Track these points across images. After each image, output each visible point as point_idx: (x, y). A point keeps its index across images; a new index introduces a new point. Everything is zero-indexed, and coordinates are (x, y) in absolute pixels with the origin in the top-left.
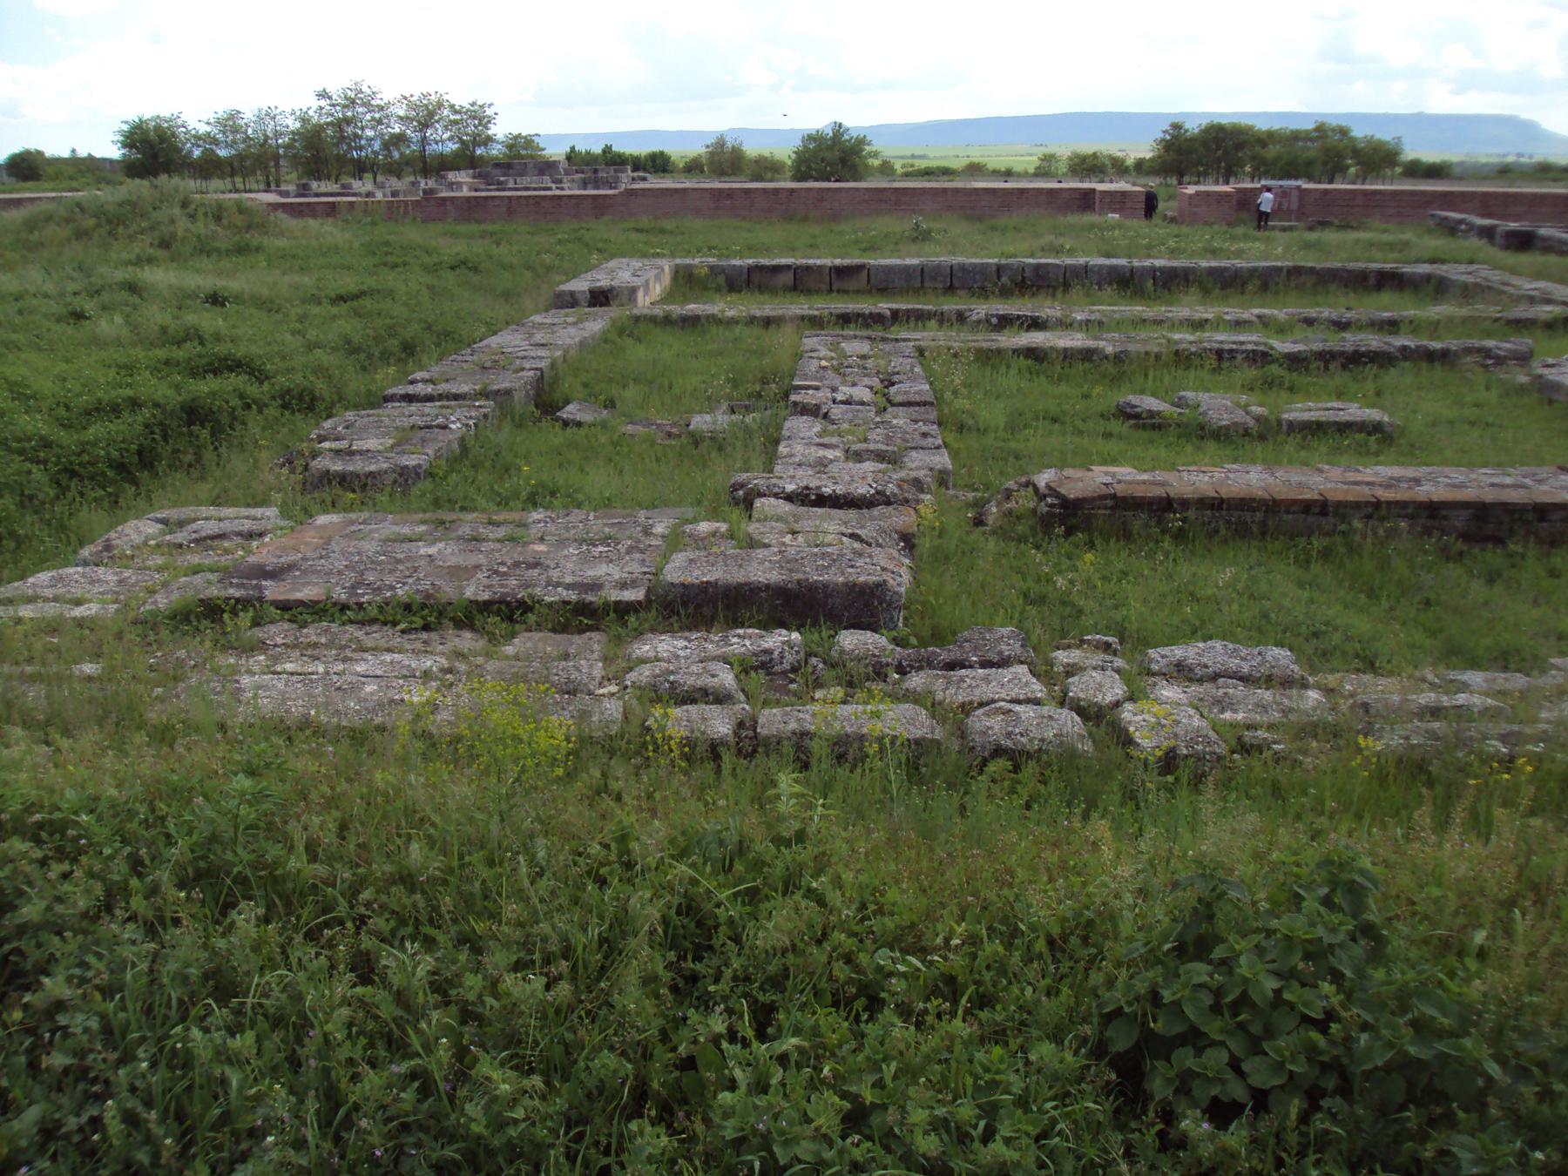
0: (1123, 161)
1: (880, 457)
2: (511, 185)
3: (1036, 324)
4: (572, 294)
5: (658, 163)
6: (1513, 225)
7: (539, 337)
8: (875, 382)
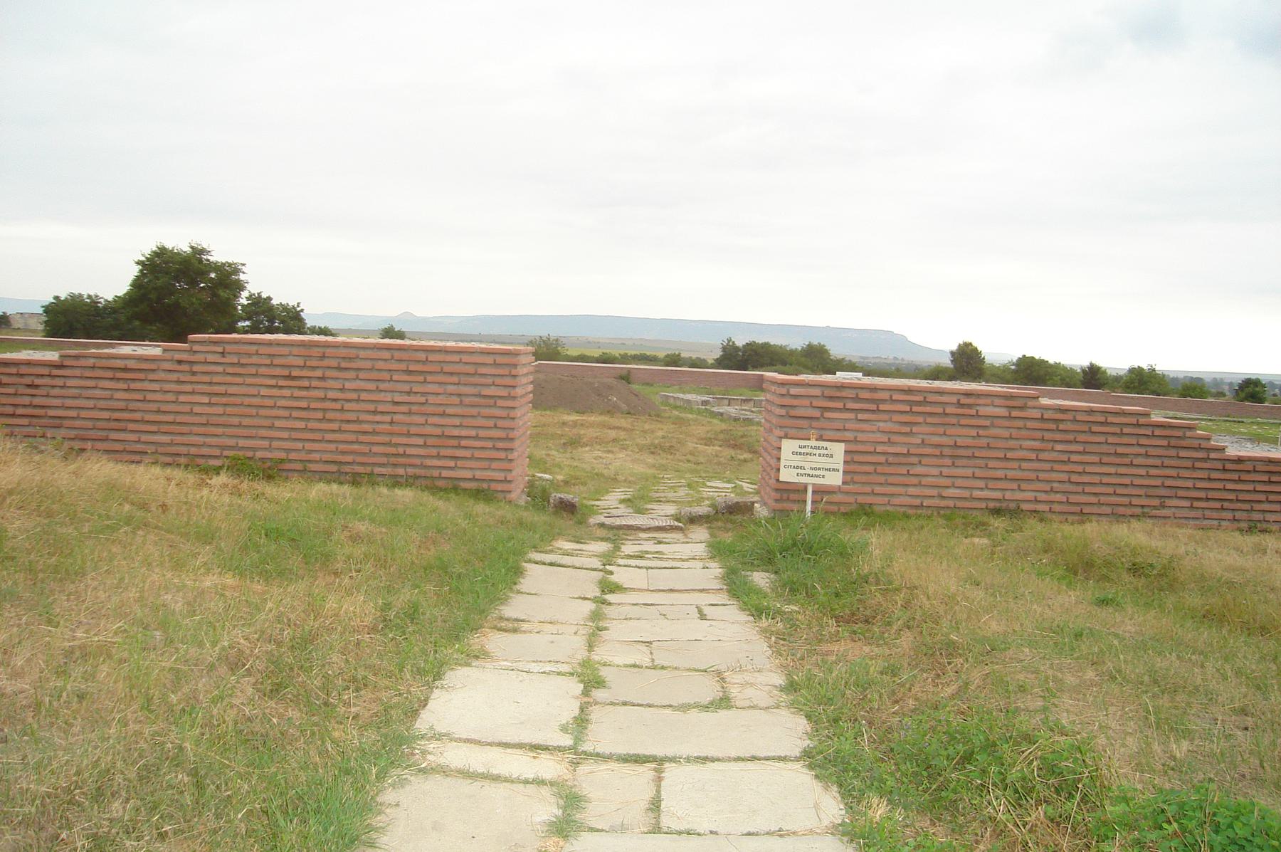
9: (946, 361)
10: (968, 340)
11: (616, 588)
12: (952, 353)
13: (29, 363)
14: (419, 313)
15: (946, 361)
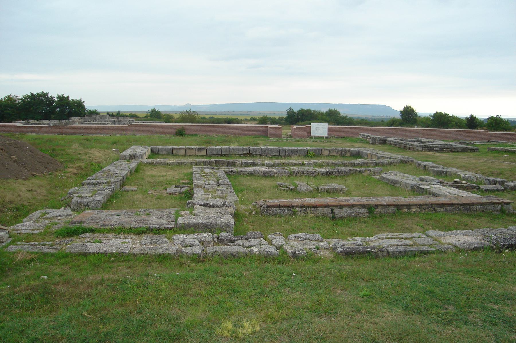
0: (275, 118)
1: (221, 197)
2: (92, 122)
3: (255, 165)
4: (125, 156)
5: (134, 116)
6: (381, 137)
7: (119, 167)
8: (216, 180)
9: (398, 116)
10: (408, 105)
11: (10, 237)
12: (401, 112)
13: (119, 257)
14: (193, 104)
15: (398, 116)
